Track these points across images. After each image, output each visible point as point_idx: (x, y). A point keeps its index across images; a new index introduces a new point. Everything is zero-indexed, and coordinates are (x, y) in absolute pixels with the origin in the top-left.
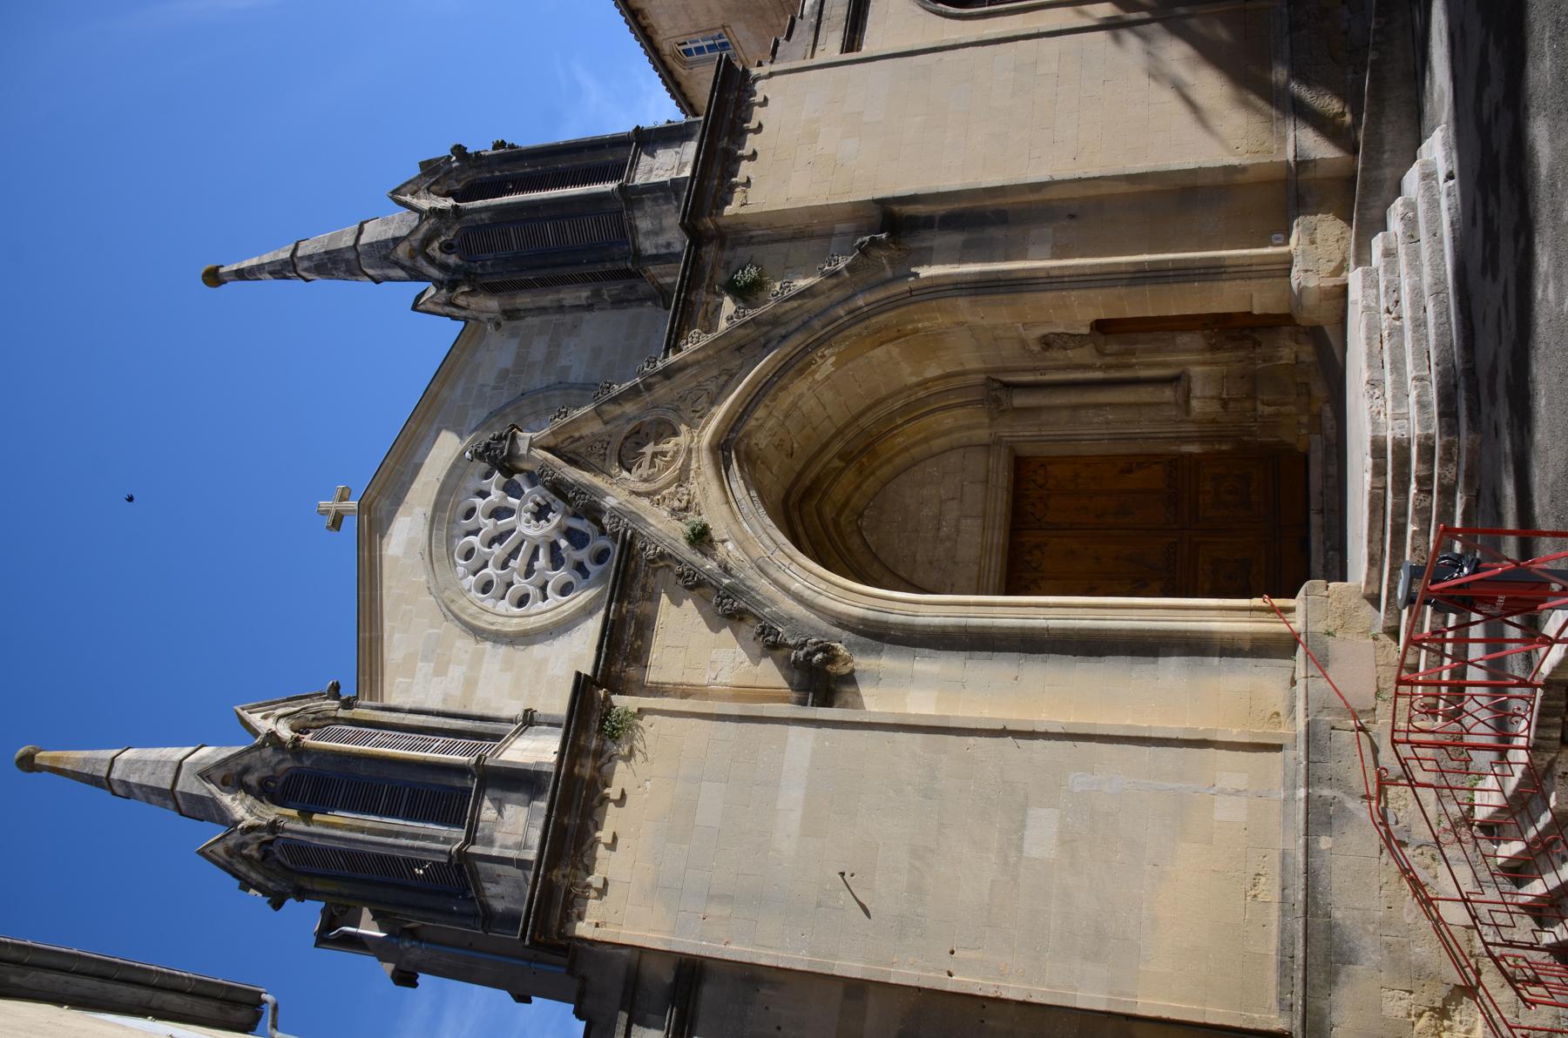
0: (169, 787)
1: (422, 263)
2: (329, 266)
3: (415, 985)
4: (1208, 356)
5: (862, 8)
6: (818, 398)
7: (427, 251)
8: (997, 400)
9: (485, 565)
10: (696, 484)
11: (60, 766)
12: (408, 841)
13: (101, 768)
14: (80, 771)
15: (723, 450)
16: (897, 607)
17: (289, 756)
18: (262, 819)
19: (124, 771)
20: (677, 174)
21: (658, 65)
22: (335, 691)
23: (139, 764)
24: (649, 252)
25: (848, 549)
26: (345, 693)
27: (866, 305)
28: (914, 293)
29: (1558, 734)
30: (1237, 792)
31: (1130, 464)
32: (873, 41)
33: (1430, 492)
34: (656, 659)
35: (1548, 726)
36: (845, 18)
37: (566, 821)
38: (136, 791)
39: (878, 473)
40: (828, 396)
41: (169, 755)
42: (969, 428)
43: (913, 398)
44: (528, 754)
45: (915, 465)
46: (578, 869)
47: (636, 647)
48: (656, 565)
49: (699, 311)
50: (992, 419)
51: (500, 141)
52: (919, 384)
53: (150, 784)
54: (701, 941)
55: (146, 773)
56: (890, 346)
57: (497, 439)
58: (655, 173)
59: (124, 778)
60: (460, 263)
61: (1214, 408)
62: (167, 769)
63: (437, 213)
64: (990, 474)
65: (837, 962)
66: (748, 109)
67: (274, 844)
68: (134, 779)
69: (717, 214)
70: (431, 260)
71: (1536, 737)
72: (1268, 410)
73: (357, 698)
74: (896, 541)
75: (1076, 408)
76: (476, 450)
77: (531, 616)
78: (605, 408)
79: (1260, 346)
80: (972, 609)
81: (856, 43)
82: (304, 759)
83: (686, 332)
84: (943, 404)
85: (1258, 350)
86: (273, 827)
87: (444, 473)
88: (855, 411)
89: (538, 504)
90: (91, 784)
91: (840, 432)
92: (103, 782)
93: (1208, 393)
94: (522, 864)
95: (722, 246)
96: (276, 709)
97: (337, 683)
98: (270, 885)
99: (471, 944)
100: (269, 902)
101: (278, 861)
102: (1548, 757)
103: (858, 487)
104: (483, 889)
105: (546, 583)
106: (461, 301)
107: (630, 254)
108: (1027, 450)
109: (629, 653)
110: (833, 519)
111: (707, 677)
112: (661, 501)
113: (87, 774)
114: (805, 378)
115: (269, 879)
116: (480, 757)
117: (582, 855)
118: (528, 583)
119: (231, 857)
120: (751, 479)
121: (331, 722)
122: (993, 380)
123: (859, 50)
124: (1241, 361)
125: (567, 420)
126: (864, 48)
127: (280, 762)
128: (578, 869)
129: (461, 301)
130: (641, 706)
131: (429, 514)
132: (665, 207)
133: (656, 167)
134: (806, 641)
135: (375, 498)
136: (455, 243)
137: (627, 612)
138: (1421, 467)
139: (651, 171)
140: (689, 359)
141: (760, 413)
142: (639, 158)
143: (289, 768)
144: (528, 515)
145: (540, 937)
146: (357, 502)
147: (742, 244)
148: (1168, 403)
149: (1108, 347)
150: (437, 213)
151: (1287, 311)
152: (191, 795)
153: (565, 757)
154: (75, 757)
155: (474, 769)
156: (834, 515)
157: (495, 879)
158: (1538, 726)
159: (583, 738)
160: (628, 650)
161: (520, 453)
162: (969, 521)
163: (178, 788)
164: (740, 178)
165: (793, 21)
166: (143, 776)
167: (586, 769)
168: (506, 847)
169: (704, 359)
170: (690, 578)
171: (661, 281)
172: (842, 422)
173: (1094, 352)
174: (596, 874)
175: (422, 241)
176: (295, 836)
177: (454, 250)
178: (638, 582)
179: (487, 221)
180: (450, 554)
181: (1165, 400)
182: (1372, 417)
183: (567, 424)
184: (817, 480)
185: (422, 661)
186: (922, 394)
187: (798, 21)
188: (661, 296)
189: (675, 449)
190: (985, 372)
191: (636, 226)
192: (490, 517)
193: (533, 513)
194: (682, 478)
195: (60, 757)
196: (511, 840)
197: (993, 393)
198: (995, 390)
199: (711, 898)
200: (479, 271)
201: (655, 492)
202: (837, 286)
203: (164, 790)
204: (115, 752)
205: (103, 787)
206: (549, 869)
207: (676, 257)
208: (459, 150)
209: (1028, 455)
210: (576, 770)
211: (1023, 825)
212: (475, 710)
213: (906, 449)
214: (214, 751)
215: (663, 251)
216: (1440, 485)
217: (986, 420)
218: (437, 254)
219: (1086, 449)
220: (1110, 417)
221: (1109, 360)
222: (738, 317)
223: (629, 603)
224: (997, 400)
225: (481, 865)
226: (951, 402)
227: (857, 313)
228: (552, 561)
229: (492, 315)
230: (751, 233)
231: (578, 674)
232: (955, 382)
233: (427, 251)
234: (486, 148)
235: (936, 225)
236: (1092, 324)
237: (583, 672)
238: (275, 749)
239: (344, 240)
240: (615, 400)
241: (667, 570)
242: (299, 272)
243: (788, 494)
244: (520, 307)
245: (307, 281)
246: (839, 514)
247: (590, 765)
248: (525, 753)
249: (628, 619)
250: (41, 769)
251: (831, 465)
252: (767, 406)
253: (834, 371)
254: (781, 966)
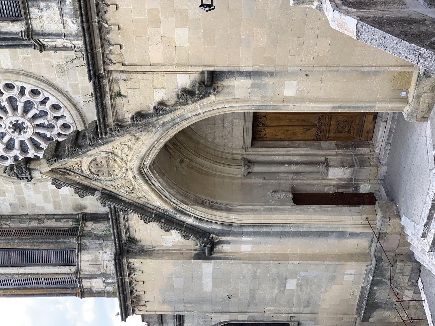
74: (205, 128)
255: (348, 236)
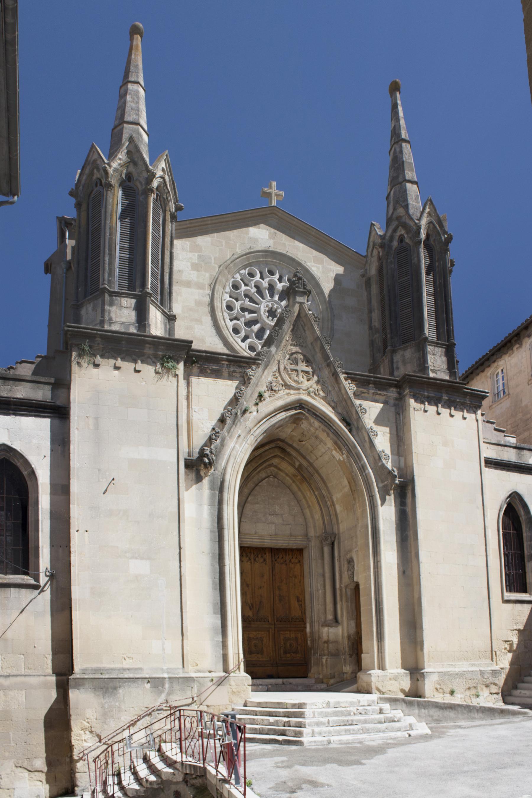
0: (125, 120)
1: (394, 224)
2: (396, 165)
3: (46, 273)
4: (346, 635)
5: (506, 468)
6: (325, 453)
7: (400, 227)
8: (326, 539)
9: (246, 285)
10: (284, 394)
11: (133, 52)
12: (107, 261)
13: (133, 76)
14: (131, 64)
15: (300, 405)
16: (231, 496)
17: (144, 187)
18: (111, 178)
19: (132, 91)
20: (431, 370)
21: (492, 352)
22: (179, 208)
23: (136, 99)
24: (394, 358)
25: (259, 472)
26: (179, 214)
27: (366, 474)
28: (371, 498)
29: (188, 772)
30: (164, 649)
31: (301, 601)
32: (491, 474)
33: (284, 726)
34: (202, 381)
35: (190, 769)
36: (502, 459)
37: (123, 343)
38: (123, 100)
39: (294, 485)
40: (326, 458)
41: (142, 115)
42: (315, 527)
43: (327, 499)
44: (154, 320)
45: (298, 502)
46: (103, 351)
47: (207, 370)
48: (245, 377)
49: (364, 389)
50: (318, 537)
51: (454, 263)
52: (333, 502)
53: (126, 108)
54: (77, 417)
55: (132, 104)
56: (348, 487)
57: (303, 284)
58: (432, 357)
59: (129, 91)
60: (393, 249)
61: (325, 638)
62: (135, 117)
63: (418, 230)
64: (294, 537)
65: (76, 480)
66: (461, 409)
67: (101, 187)
68: (128, 98)
69: (411, 395)
70: (395, 231)
71: (186, 764)
72: (324, 661)
73: (176, 222)
75: (324, 576)
76: (298, 272)
77: (222, 313)
78: (319, 342)
79: (350, 657)
80: (232, 531)
81: (489, 465)
82: (143, 196)
83: (355, 383)
84: (324, 514)
85: (348, 656)
86: (109, 186)
87: (290, 255)
88: (320, 471)
89: (276, 310)
90: (125, 73)
91: (311, 464)
92: (126, 81)
93: (330, 635)
94: (102, 322)
95: (396, 399)
96: (168, 175)
97: (183, 209)
98: (81, 188)
99: (68, 299)
100: (72, 189)
101: (92, 191)
102: (180, 769)
103: (287, 475)
104: (90, 303)
105: (238, 320)
106: (375, 252)
107: (394, 348)
108: (306, 554)
109: (204, 367)
110: (273, 464)
111: (195, 407)
112: (275, 376)
113: (130, 69)
114: (333, 446)
115: (83, 187)
116: (150, 294)
117: (109, 352)
118: (238, 310)
119: (92, 163)
120: (287, 422)
121: (163, 208)
122: (335, 537)
123: (486, 466)
124: (344, 648)
125: (313, 322)
126: (487, 469)
127: (141, 183)
128: (103, 351)
129: (375, 252)
130: (179, 375)
131: (271, 249)
132: (415, 365)
133: (435, 357)
134: (213, 454)
135: (277, 216)
136: (403, 243)
137: (223, 364)
138: (294, 723)
139: (434, 354)
140: (341, 385)
141: (317, 424)
142: (440, 347)
143: (138, 188)
144: (270, 306)
145: (69, 335)
146: (275, 205)
147: (396, 409)
148: (326, 617)
149: (349, 590)
150: (418, 230)
151: (363, 668)
152: (122, 134)
153: (153, 339)
154: (138, 59)
155: (144, 291)
156: (274, 464)
157: (95, 309)
158: (190, 765)
159: (162, 347)
160: (205, 366)
161: (297, 297)
162: (273, 528)
163: (125, 125)
164: (428, 407)
165: (503, 431)
166: (130, 103)
167: (148, 350)
168: (109, 313)
169: (342, 393)
170: (239, 395)
171: (382, 366)
172: (315, 465)
173: (347, 584)
174: (101, 360)
175: (405, 223)
176: (105, 197)
177: (400, 243)
178: (236, 368)
179: (413, 261)
180: (250, 265)
181: (327, 616)
182: (314, 703)
183: (311, 322)
184: (289, 454)
185: (198, 255)
186: (329, 503)
187: (503, 434)
188: (374, 368)
189: (300, 382)
190: (338, 533)
191: (407, 349)
192: (269, 285)
193: (272, 308)
194: (288, 386)
195: (138, 50)
196: (113, 315)
197: (329, 538)
198: (331, 537)
199: (97, 419)
200: (389, 260)
201: (279, 372)
202: (375, 459)
203: (124, 118)
204: (142, 83)
205: (124, 80)
206: (101, 336)
207: (392, 373)
208: (450, 239)
209: (304, 554)
210: (148, 345)
211: (142, 559)
212: (175, 288)
213: (305, 497)
214: (145, 143)
215: (395, 366)
216: (286, 730)
217: (318, 535)
218: (398, 234)
219: (307, 580)
220: (320, 591)
221: (344, 590)
222: (361, 410)
223: (227, 365)
224: (326, 539)
225: (100, 301)
226: (325, 517)
227: (362, 470)
228: (249, 322)
229: (368, 272)
230: (401, 414)
231: (191, 342)
232: (334, 520)
233: (400, 227)
234: (450, 256)
235: (402, 508)
236: (358, 582)
237: (193, 344)
238: (147, 178)
239: (409, 172)
240: (322, 348)
241: (243, 383)
242: (394, 146)
243: (283, 441)
244: (372, 287)
245: (390, 153)
246: (275, 467)
247: (150, 352)
248: (154, 318)
249: (219, 365)
250: (132, 40)
251: (296, 461)
252: (320, 427)
253: (337, 460)
254: (71, 455)
255: (216, 639)
